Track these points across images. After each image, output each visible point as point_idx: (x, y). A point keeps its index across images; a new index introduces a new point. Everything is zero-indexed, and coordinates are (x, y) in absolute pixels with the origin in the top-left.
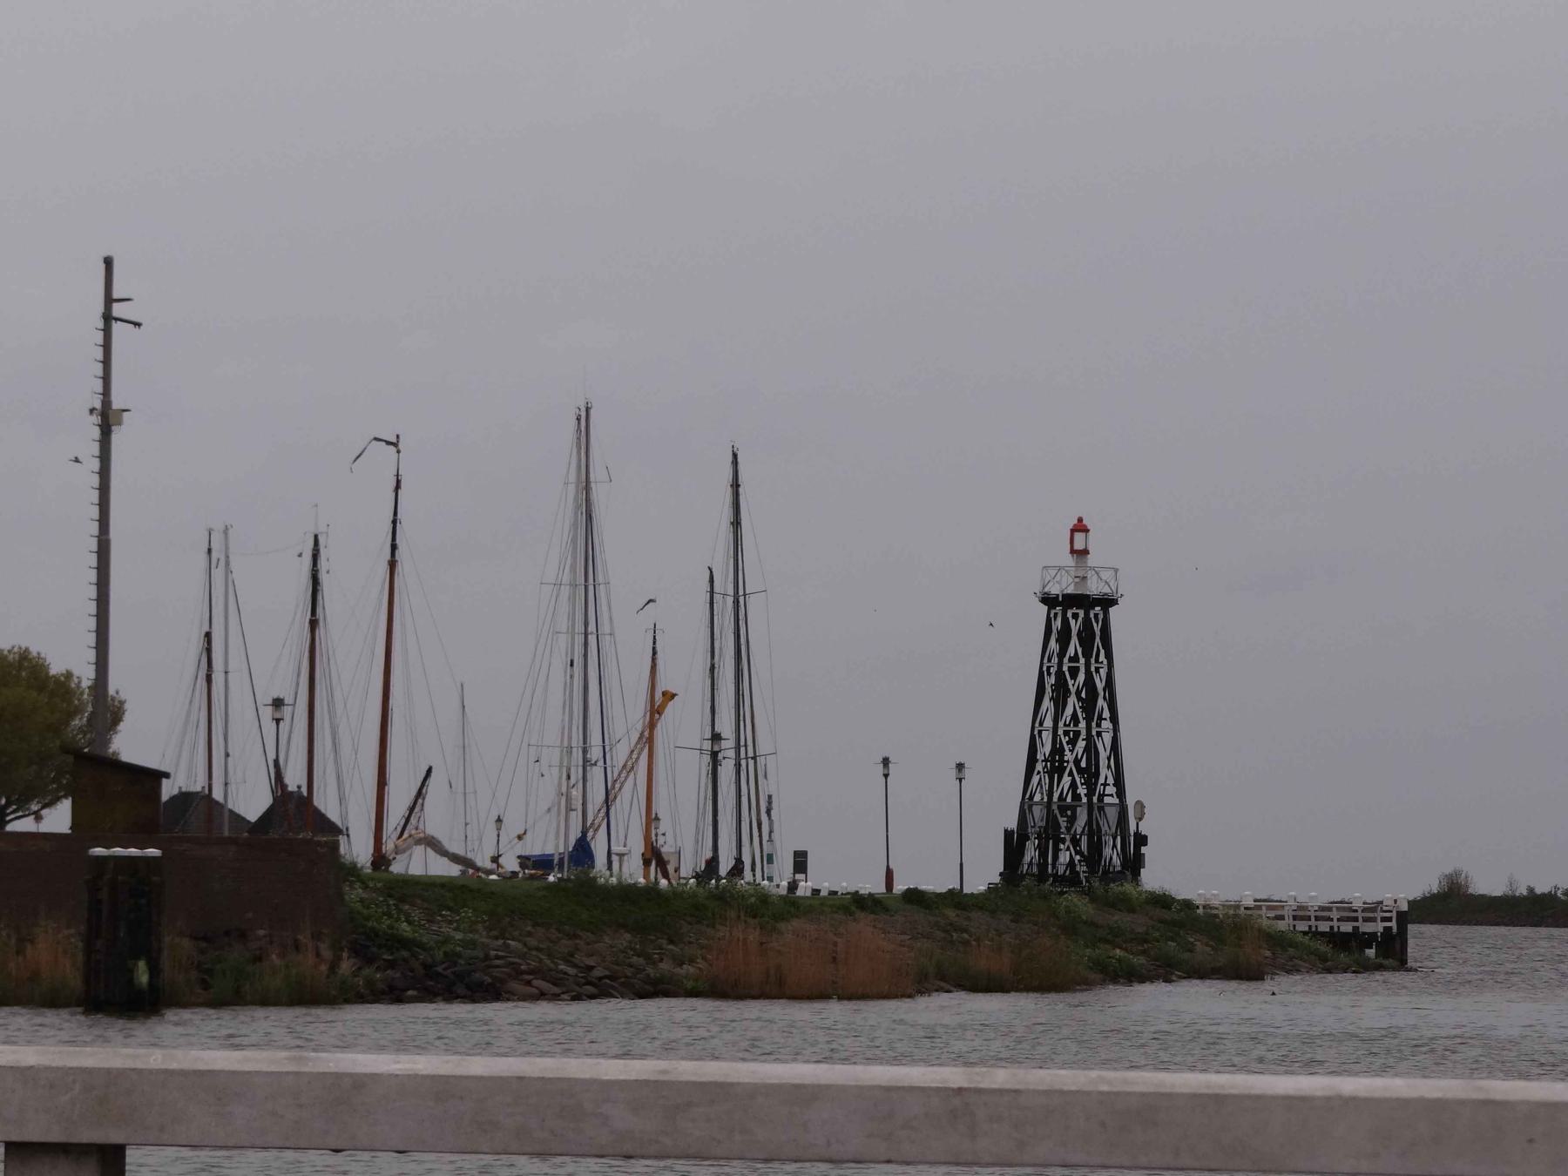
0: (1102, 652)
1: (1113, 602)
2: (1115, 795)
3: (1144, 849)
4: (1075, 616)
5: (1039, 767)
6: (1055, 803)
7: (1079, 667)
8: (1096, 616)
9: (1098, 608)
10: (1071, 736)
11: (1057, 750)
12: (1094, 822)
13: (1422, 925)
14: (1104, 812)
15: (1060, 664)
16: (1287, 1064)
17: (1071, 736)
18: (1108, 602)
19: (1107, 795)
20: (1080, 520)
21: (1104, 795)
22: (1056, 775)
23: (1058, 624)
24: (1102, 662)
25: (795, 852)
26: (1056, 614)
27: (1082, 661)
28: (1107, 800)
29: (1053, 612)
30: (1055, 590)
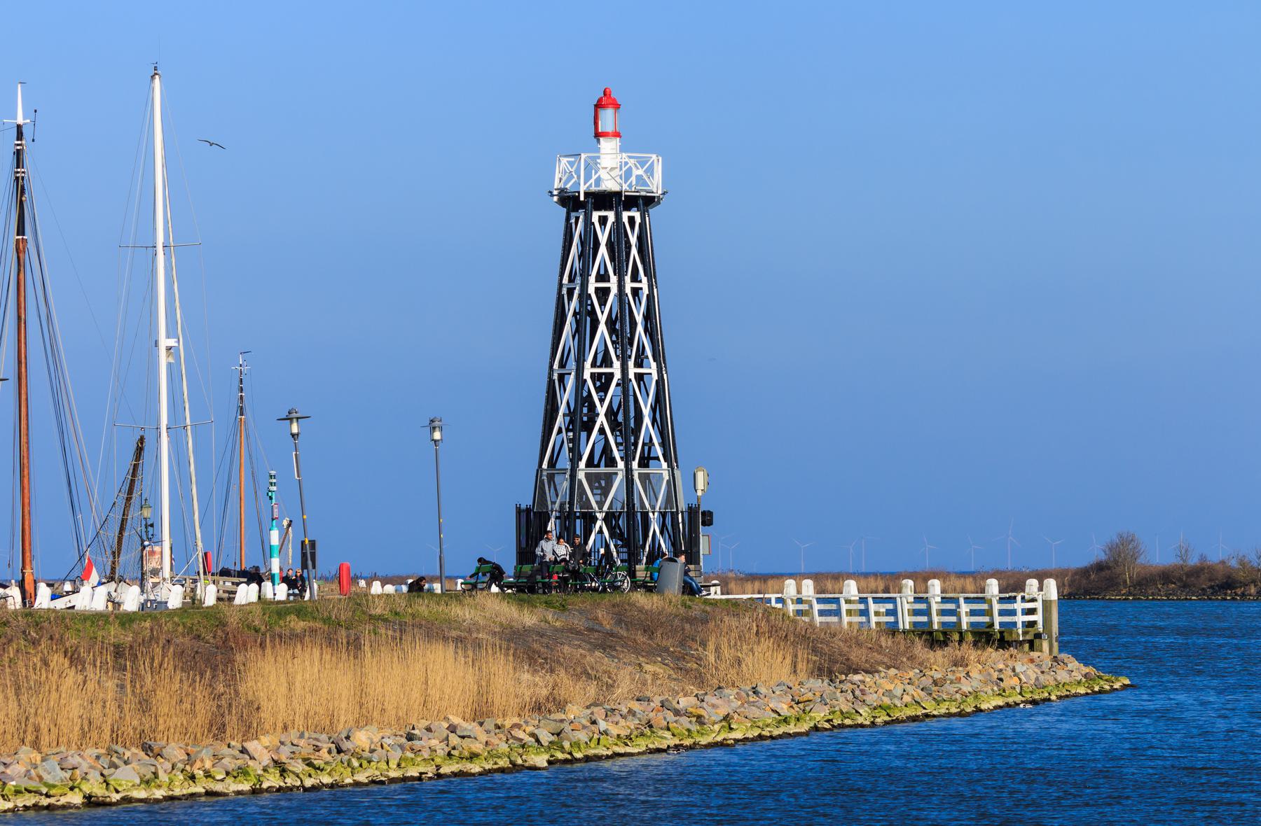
4: (603, 221)
5: (560, 421)
6: (583, 470)
7: (609, 288)
8: (632, 220)
12: (631, 399)
15: (580, 370)
23: (579, 229)
26: (577, 219)
27: (614, 279)
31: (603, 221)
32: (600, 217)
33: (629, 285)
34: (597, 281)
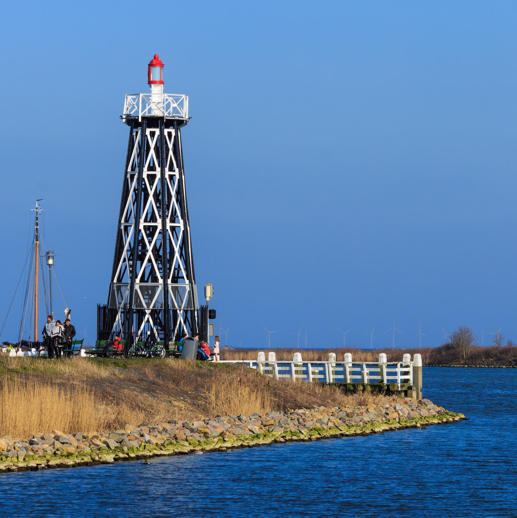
6: (138, 284)
8: (170, 134)
11: (139, 242)
13: (183, 455)
14: (178, 292)
16: (191, 294)
22: (197, 332)
26: (137, 133)
31: (153, 134)
32: (150, 132)
33: (167, 173)
34: (148, 170)
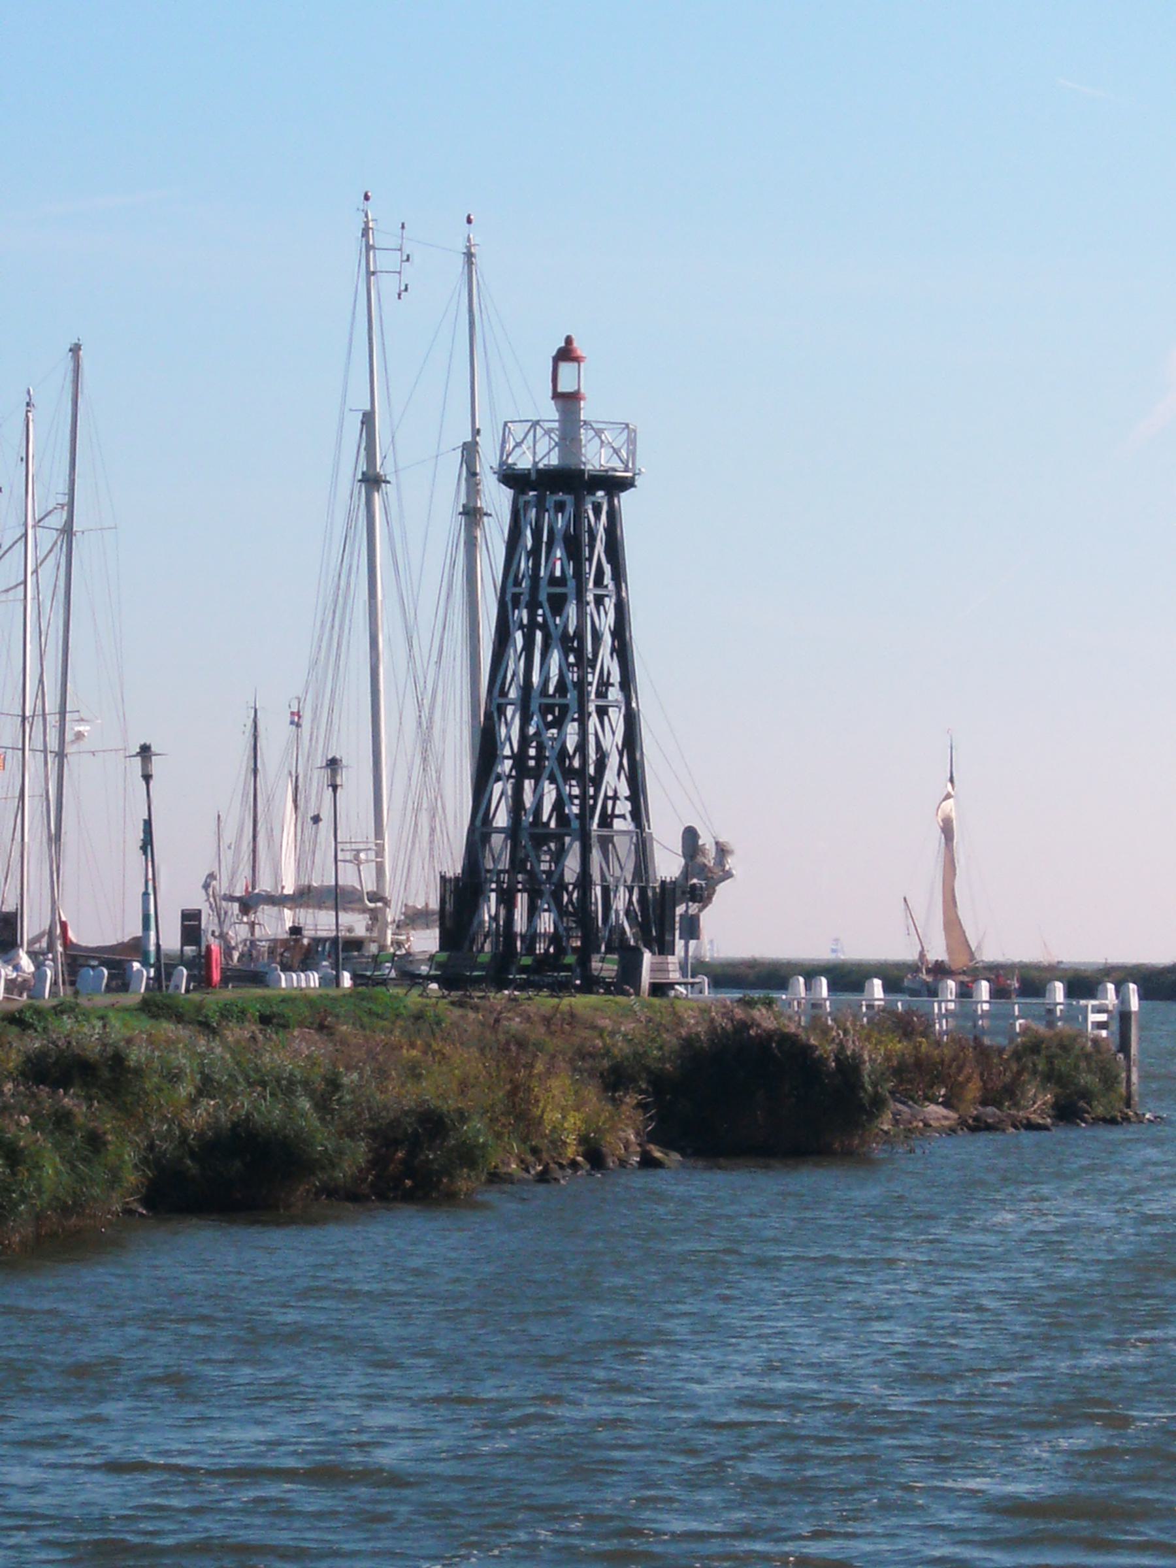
0: (607, 568)
1: (625, 484)
2: (628, 816)
3: (478, 439)
9: (600, 493)
10: (557, 714)
17: (557, 714)
18: (615, 485)
19: (618, 816)
20: (569, 340)
21: (613, 816)
24: (606, 587)
25: (183, 911)
28: (618, 824)
29: (522, 499)
30: (523, 461)
